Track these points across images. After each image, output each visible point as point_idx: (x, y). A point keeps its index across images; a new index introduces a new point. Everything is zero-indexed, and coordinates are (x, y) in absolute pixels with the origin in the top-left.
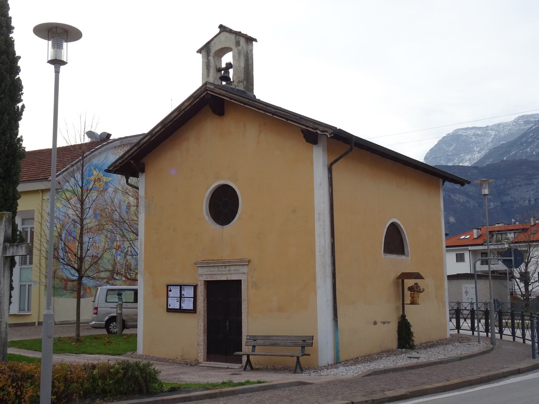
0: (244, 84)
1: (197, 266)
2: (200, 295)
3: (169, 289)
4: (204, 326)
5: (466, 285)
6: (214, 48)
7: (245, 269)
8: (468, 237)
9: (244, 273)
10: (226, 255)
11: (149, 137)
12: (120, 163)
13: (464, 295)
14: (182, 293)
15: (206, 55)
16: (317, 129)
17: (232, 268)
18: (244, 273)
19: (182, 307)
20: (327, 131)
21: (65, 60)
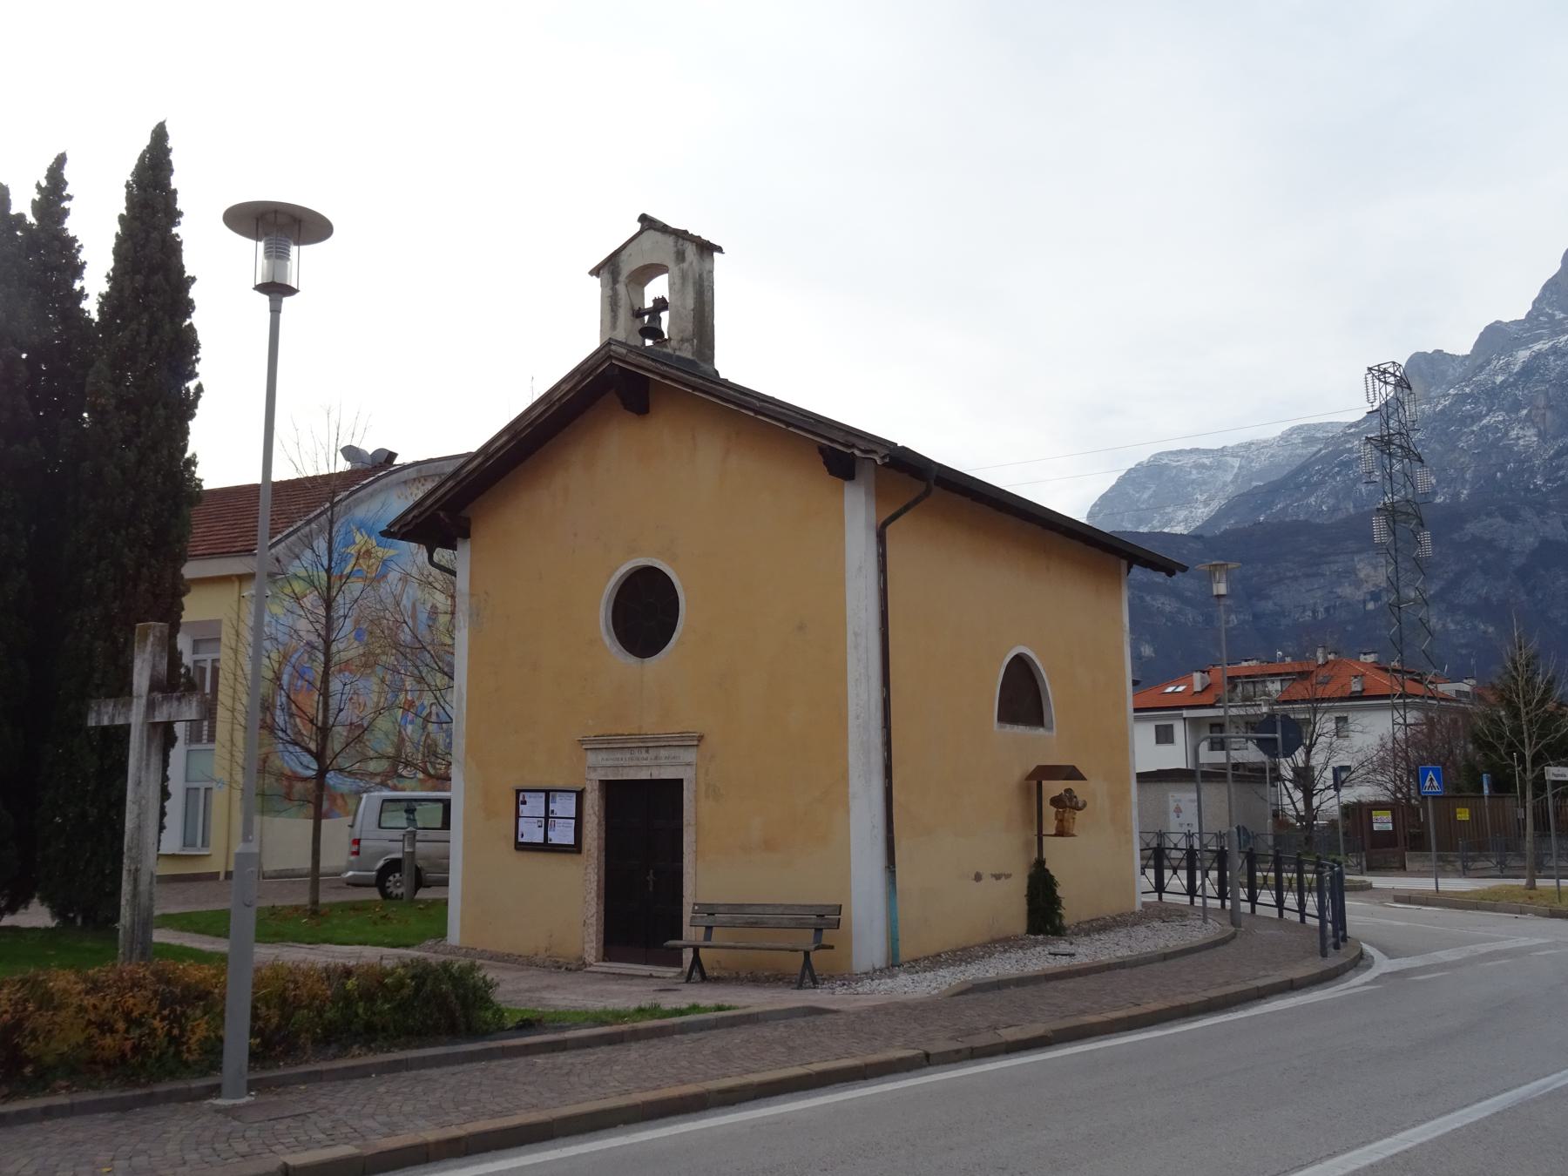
0: (692, 345)
1: (584, 747)
2: (591, 812)
3: (521, 798)
4: (599, 881)
5: (1178, 795)
6: (628, 266)
7: (690, 756)
8: (1181, 689)
9: (688, 764)
10: (650, 724)
11: (479, 460)
12: (414, 517)
13: (1173, 816)
15: (611, 280)
17: (663, 753)
18: (688, 764)
19: (550, 840)
20: (875, 452)
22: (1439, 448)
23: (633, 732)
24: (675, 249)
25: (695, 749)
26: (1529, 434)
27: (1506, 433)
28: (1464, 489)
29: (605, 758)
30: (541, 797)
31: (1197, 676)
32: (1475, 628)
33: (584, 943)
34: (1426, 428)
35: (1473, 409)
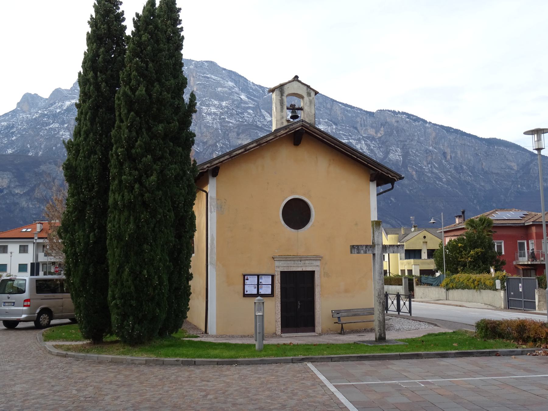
3: (246, 278)
7: (318, 263)
8: (29, 230)
10: (301, 252)
11: (242, 150)
12: (208, 167)
14: (260, 281)
15: (280, 94)
16: (389, 174)
17: (307, 262)
19: (260, 293)
21: (544, 147)
22: (32, 133)
23: (294, 255)
24: (307, 91)
25: (320, 261)
26: (67, 134)
27: (59, 132)
28: (40, 151)
29: (283, 263)
30: (255, 278)
31: (38, 226)
32: (40, 207)
33: (276, 328)
34: (28, 124)
35: (47, 120)
